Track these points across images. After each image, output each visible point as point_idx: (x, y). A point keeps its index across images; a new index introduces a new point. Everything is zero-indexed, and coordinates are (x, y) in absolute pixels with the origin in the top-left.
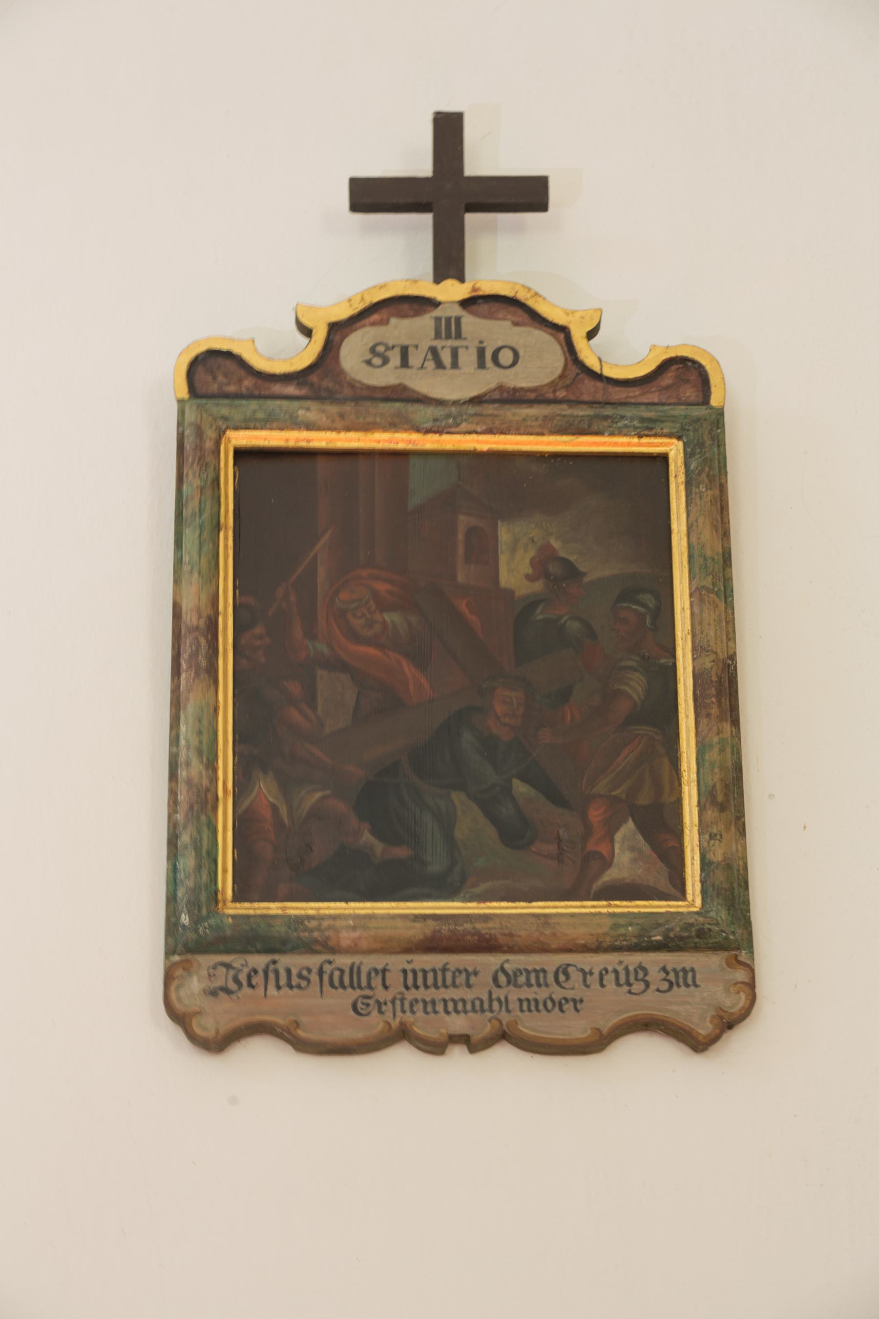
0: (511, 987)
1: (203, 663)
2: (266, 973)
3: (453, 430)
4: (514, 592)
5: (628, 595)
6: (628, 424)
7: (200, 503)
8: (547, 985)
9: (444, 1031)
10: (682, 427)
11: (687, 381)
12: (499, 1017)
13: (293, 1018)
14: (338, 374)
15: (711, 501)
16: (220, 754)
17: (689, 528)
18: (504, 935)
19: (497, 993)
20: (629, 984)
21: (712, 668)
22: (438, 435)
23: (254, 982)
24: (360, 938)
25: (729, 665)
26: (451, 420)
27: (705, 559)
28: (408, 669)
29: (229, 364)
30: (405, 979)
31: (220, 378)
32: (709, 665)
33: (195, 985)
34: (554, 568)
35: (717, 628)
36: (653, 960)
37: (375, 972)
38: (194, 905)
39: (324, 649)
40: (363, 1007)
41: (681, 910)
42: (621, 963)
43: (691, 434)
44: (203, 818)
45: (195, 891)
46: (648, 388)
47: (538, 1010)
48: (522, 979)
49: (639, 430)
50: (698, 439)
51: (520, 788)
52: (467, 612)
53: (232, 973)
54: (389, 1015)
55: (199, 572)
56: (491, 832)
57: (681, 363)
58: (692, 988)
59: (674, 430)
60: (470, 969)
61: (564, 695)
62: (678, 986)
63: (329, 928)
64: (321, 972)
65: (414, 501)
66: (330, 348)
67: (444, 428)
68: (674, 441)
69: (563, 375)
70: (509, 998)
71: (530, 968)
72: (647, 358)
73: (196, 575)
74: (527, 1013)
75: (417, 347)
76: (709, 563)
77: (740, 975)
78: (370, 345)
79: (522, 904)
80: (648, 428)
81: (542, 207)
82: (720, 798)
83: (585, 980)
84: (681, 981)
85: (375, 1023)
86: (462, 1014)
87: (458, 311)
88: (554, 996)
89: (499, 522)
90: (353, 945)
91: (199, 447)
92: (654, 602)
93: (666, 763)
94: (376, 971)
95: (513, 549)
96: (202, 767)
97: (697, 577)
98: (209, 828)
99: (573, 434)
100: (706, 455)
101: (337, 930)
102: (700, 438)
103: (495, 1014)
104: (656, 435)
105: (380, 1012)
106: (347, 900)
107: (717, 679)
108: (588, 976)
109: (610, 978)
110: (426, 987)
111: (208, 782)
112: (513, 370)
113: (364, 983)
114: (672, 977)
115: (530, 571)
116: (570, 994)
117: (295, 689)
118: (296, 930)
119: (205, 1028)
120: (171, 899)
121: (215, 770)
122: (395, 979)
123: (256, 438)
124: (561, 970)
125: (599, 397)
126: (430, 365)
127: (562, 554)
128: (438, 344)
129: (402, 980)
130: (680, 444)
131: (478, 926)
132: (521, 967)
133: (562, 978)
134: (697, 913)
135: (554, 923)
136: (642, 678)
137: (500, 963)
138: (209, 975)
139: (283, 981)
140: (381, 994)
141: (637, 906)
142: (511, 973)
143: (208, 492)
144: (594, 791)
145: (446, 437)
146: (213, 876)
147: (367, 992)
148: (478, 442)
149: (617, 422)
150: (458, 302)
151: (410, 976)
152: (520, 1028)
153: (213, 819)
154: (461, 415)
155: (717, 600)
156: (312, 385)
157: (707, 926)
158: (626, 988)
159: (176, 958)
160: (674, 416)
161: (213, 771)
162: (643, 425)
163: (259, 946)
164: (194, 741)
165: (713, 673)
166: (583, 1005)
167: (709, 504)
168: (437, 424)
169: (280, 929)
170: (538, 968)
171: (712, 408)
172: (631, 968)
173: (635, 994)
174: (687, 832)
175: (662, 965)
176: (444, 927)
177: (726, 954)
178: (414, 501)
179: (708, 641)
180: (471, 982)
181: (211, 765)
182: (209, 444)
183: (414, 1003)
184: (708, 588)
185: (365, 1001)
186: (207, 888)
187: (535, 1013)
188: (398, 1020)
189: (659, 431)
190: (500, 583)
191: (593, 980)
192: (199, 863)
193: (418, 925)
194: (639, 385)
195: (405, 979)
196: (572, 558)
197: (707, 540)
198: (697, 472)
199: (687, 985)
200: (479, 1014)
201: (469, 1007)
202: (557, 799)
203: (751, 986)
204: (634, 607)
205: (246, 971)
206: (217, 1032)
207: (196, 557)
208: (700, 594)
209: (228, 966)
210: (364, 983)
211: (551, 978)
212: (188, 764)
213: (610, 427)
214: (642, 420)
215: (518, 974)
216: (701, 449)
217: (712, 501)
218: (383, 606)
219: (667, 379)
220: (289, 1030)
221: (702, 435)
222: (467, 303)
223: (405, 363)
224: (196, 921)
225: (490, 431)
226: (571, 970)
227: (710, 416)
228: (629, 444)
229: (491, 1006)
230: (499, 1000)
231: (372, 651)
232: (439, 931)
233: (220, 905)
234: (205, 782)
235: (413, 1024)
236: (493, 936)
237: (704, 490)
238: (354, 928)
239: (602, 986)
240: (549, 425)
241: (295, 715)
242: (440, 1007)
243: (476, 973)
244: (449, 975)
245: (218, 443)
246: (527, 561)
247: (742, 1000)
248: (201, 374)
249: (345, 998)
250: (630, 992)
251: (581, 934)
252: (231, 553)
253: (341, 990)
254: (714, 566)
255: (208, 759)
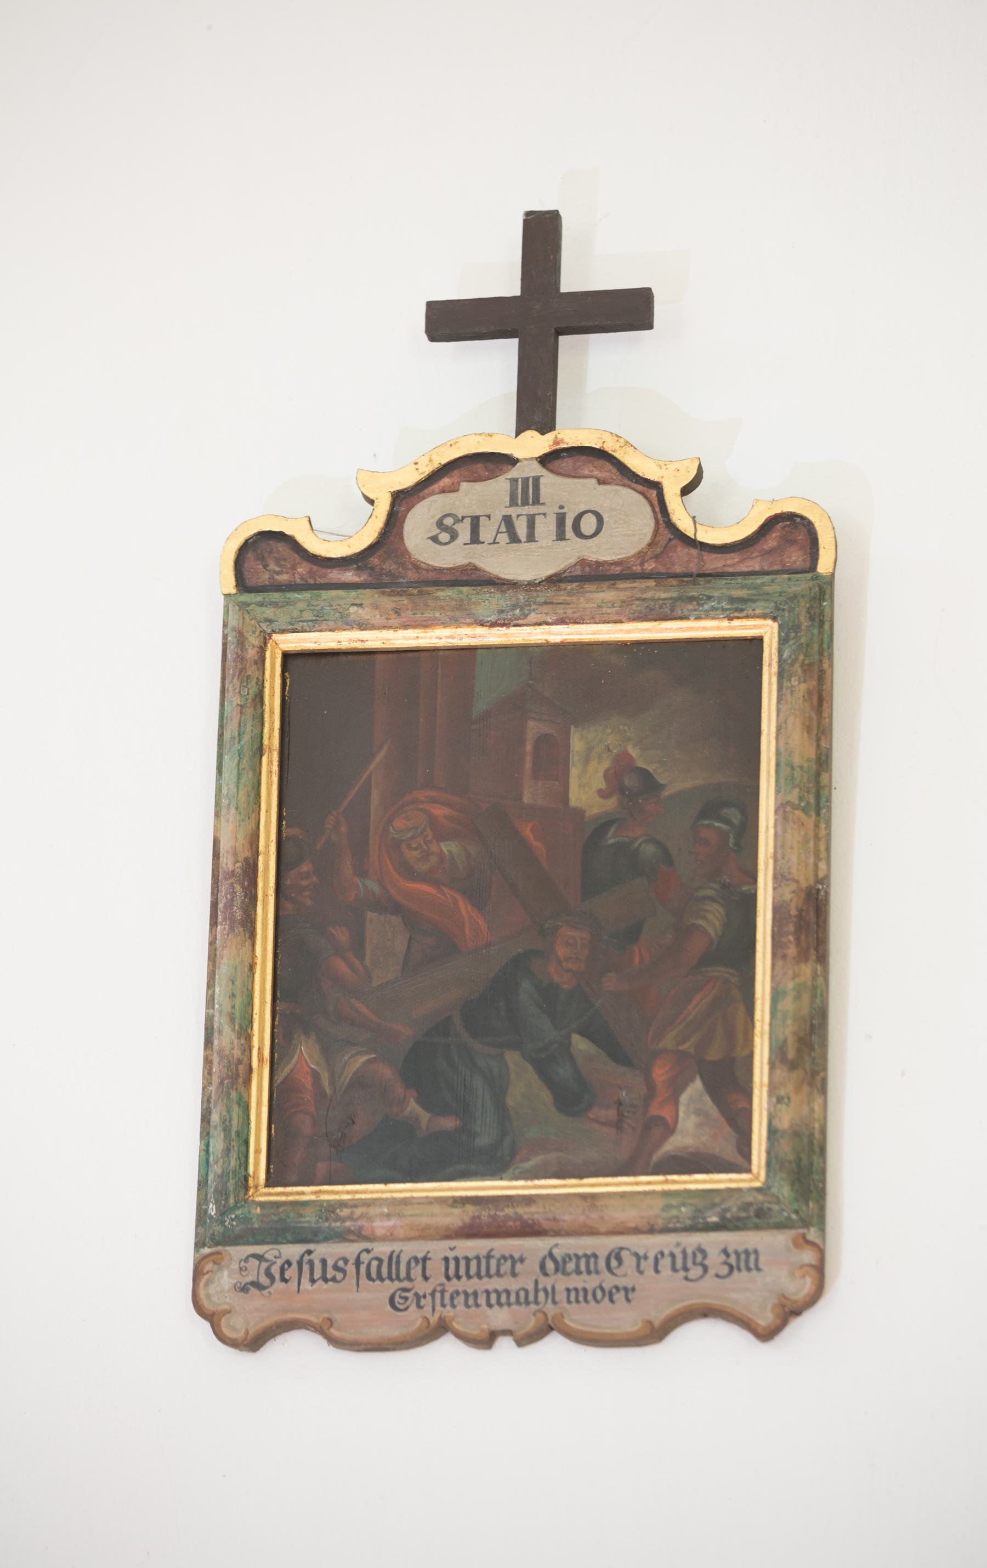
0: (559, 1275)
1: (238, 914)
2: (300, 1264)
3: (520, 622)
4: (584, 812)
5: (710, 810)
6: (716, 606)
7: (240, 724)
8: (597, 1272)
9: (485, 1327)
10: (777, 606)
11: (793, 542)
12: (545, 1310)
13: (327, 1315)
14: (400, 554)
15: (804, 696)
16: (256, 1017)
17: (779, 729)
18: (548, 1219)
19: (545, 1282)
20: (686, 1269)
21: (791, 900)
22: (504, 628)
23: (287, 1276)
24: (394, 1227)
25: (818, 890)
26: (517, 612)
27: (792, 768)
28: (465, 908)
29: (281, 547)
30: (447, 1268)
31: (273, 566)
32: (788, 896)
33: (225, 1280)
34: (630, 781)
35: (801, 851)
36: (713, 1241)
37: (415, 1261)
38: (222, 1193)
39: (374, 886)
40: (402, 1301)
41: (742, 1185)
42: (678, 1244)
43: (787, 614)
44: (234, 1094)
45: (223, 1176)
46: (749, 554)
47: (586, 1300)
48: (571, 1266)
49: (728, 612)
50: (794, 621)
51: (580, 1044)
52: (532, 838)
53: (264, 1265)
54: (428, 1309)
55: (237, 808)
56: (546, 1096)
57: (788, 520)
58: (754, 1273)
59: (768, 611)
60: (516, 1256)
61: (633, 933)
62: (739, 1270)
63: (362, 1216)
64: (358, 1262)
65: (480, 707)
66: (394, 522)
67: (511, 620)
68: (769, 622)
69: (652, 542)
70: (557, 1287)
71: (580, 1253)
72: (749, 516)
73: (233, 811)
74: (574, 1305)
75: (489, 517)
76: (797, 773)
77: (808, 1256)
78: (438, 517)
79: (573, 1181)
80: (738, 610)
81: (647, 324)
82: (791, 1054)
83: (638, 1265)
84: (742, 1264)
85: (413, 1319)
86: (506, 1307)
87: (537, 470)
88: (604, 1285)
89: (572, 728)
90: (389, 1234)
91: (241, 658)
92: (739, 817)
93: (741, 1009)
94: (416, 1259)
95: (586, 761)
96: (234, 1036)
97: (783, 790)
98: (239, 1104)
99: (655, 620)
100: (802, 640)
101: (370, 1219)
102: (796, 620)
103: (540, 1307)
104: (747, 617)
105: (419, 1306)
106: (386, 1181)
107: (797, 913)
108: (642, 1261)
109: (666, 1262)
110: (469, 1277)
111: (239, 1053)
112: (596, 539)
113: (403, 1274)
114: (733, 1260)
115: (603, 786)
116: (621, 1282)
117: (342, 935)
118: (327, 1220)
119: (234, 1329)
120: (202, 1184)
121: (249, 1038)
122: (437, 1268)
123: (304, 640)
124: (613, 1255)
125: (693, 568)
126: (504, 538)
127: (640, 764)
128: (513, 512)
129: (443, 1269)
130: (776, 625)
131: (520, 1210)
132: (571, 1252)
133: (614, 1263)
134: (758, 1190)
135: (602, 1206)
136: (721, 910)
137: (548, 1247)
138: (241, 1269)
139: (318, 1274)
140: (422, 1287)
141: (696, 1182)
142: (559, 1259)
143: (249, 711)
144: (660, 1046)
145: (513, 630)
146: (243, 1160)
147: (406, 1284)
148: (550, 633)
149: (703, 605)
150: (536, 459)
151: (452, 1265)
152: (567, 1321)
153: (245, 1096)
154: (530, 605)
155: (803, 816)
156: (372, 569)
157: (766, 1205)
158: (682, 1274)
159: (206, 1250)
160: (768, 594)
161: (246, 1039)
162: (733, 607)
163: (289, 1237)
164: (227, 1007)
165: (793, 906)
166: (636, 1294)
167: (801, 700)
168: (503, 616)
169: (309, 1219)
170: (589, 1252)
171: (818, 577)
172: (689, 1251)
173: (692, 1280)
174: (756, 1092)
175: (722, 1247)
176: (483, 1213)
177: (792, 1233)
178: (480, 707)
179: (789, 868)
180: (517, 1270)
181: (245, 1033)
182: (251, 653)
183: (455, 1295)
184: (793, 803)
185: (404, 1294)
186: (235, 1175)
187: (583, 1304)
188: (437, 1316)
189: (750, 612)
190: (570, 803)
191: (647, 1265)
192: (228, 1147)
193: (456, 1211)
194: (739, 550)
195: (447, 1268)
196: (650, 768)
197: (796, 745)
198: (789, 661)
199: (749, 1269)
200: (524, 1306)
201: (513, 1299)
202: (618, 1055)
203: (820, 1270)
204: (717, 824)
205: (279, 1262)
206: (247, 1332)
207: (233, 787)
208: (785, 811)
209: (260, 1258)
210: (403, 1274)
211: (602, 1264)
212: (220, 1032)
213: (695, 610)
214: (732, 600)
215: (567, 1260)
216: (796, 633)
217: (806, 697)
218: (441, 836)
219: (771, 542)
220: (321, 1328)
221: (798, 615)
222: (546, 460)
223: (475, 538)
224: (224, 1211)
225: (562, 621)
226: (624, 1254)
227: (810, 589)
228: (718, 628)
229: (536, 1297)
230: (545, 1290)
231: (426, 888)
232: (479, 1217)
233: (251, 1191)
234: (237, 1053)
235: (453, 1319)
236: (536, 1222)
237: (796, 683)
238: (388, 1216)
239: (657, 1271)
240: (627, 612)
241: (342, 967)
242: (482, 1300)
243: (522, 1260)
244: (493, 1263)
245: (262, 650)
246: (601, 774)
247: (807, 1286)
248: (251, 562)
249: (381, 1291)
250: (686, 1278)
251: (630, 1216)
252: (275, 779)
253: (378, 1282)
254: (802, 776)
255: (241, 1026)
